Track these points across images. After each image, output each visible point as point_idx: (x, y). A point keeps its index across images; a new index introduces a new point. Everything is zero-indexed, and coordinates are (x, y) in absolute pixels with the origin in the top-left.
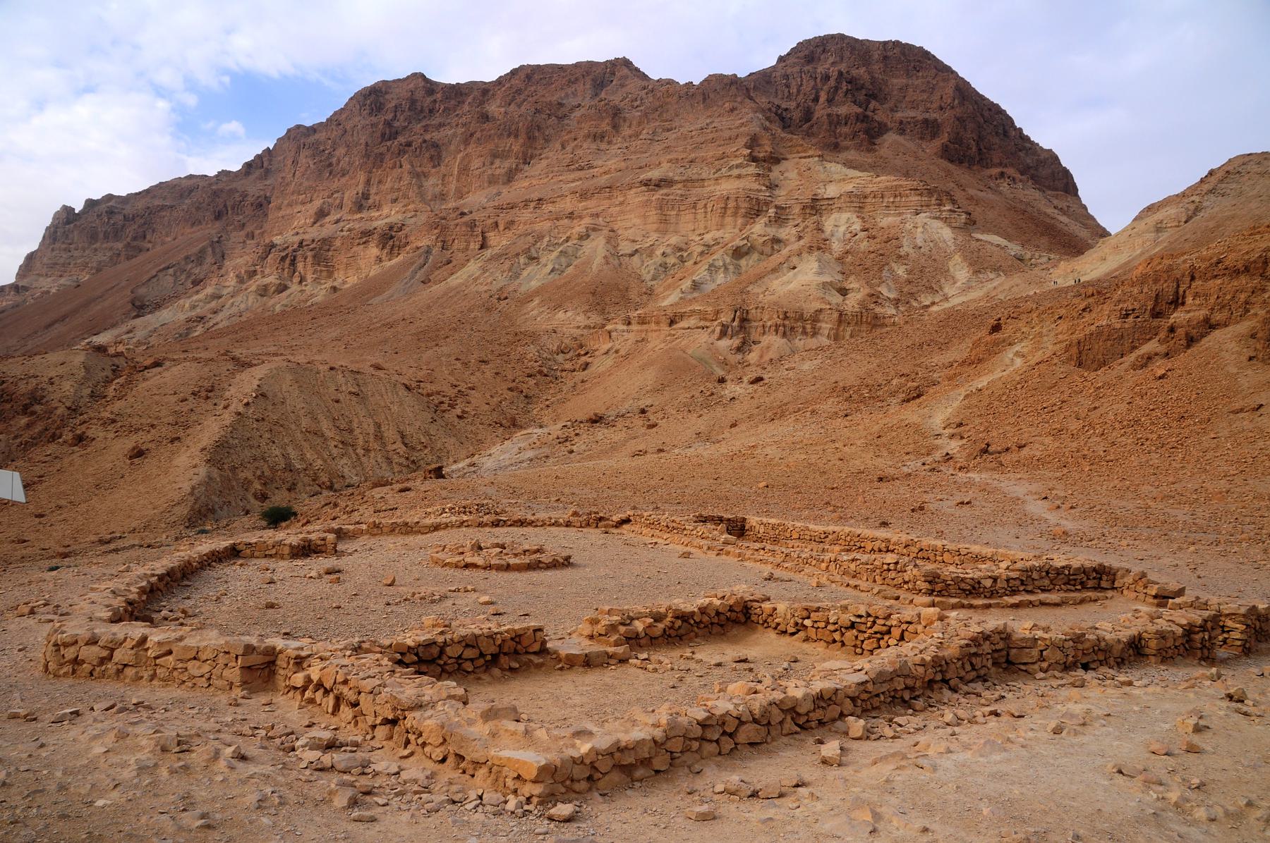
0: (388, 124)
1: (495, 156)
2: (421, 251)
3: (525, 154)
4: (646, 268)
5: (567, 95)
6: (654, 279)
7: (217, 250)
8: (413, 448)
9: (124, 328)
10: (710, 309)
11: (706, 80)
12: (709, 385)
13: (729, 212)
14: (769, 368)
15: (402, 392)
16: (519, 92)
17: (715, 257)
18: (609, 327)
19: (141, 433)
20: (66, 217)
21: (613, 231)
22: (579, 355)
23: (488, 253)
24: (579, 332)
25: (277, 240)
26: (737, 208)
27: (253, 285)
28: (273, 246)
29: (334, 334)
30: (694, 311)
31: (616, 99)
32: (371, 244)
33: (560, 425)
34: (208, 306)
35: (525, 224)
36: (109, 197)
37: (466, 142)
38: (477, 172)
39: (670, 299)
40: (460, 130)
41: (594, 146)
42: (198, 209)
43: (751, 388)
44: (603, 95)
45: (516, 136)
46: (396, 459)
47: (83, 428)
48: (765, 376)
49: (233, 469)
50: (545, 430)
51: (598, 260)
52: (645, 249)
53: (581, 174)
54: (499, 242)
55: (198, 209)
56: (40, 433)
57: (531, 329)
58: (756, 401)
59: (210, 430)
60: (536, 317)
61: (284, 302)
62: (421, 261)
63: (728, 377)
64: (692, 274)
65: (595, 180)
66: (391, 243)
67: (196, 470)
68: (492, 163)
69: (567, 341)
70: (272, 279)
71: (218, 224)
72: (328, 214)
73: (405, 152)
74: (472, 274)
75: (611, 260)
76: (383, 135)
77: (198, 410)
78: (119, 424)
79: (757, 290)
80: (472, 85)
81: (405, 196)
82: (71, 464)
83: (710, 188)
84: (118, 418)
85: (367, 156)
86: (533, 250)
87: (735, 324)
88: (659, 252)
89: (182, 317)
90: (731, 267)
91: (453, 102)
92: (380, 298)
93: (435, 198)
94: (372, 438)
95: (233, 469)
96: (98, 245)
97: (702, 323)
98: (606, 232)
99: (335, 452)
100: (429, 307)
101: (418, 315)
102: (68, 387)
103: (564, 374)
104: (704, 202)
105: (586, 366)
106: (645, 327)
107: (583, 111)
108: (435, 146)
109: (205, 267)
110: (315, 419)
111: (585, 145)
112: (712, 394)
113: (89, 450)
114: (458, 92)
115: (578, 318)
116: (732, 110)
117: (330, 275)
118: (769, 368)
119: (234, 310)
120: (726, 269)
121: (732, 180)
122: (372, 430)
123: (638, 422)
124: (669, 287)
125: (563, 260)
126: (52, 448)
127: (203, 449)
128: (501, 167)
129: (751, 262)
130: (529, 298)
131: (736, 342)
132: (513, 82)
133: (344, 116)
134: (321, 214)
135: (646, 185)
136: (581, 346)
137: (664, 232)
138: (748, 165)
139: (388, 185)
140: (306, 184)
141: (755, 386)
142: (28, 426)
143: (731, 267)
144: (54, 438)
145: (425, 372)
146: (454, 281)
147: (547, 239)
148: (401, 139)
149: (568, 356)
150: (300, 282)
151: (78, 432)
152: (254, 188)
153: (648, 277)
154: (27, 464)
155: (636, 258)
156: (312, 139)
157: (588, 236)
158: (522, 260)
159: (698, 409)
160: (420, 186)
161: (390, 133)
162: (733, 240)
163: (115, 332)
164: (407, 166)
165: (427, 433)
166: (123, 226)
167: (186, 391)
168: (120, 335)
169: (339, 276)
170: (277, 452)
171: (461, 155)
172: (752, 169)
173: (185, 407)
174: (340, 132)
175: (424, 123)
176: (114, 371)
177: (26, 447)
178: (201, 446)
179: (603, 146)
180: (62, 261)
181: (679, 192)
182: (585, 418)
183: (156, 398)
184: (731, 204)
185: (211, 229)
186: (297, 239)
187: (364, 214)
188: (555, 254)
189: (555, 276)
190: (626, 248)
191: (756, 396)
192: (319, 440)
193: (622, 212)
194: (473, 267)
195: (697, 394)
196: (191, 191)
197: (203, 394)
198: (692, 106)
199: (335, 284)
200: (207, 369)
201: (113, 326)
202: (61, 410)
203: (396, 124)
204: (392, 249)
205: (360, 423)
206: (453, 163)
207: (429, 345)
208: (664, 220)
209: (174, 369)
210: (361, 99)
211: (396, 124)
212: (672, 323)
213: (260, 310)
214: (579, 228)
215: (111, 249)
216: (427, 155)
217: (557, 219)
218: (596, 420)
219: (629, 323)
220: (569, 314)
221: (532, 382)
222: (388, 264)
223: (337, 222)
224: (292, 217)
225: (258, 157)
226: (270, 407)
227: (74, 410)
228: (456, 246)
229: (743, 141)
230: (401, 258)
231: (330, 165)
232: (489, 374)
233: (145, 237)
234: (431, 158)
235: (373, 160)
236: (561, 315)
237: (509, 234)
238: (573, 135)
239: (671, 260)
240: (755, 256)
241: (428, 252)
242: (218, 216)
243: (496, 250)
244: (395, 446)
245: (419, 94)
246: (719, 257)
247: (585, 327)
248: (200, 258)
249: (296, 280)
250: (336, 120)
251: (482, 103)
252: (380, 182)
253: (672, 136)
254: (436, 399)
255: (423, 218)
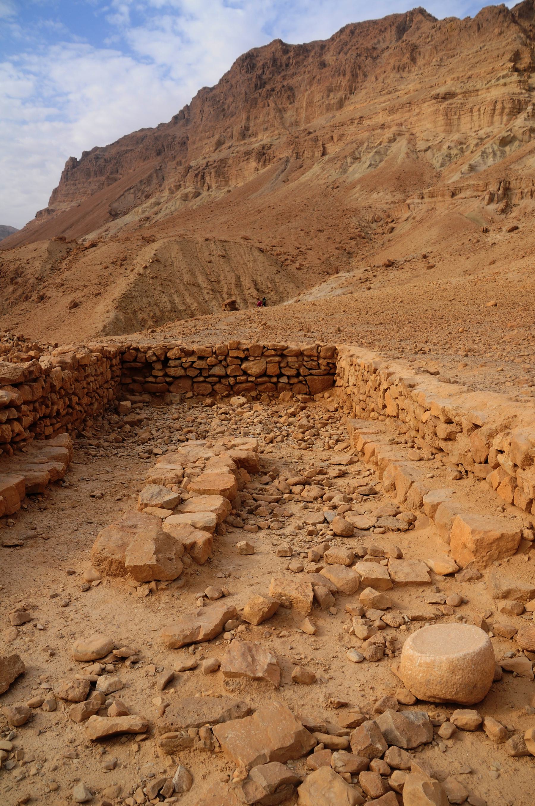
0: (259, 77)
1: (330, 90)
2: (282, 160)
3: (350, 87)
4: (435, 160)
5: (379, 42)
6: (442, 165)
7: (160, 175)
8: (263, 292)
9: (104, 228)
10: (481, 183)
11: (481, 13)
12: (476, 235)
13: (497, 112)
14: (523, 219)
15: (257, 253)
16: (346, 44)
17: (486, 146)
18: (408, 202)
19: (78, 291)
20: (73, 164)
21: (412, 134)
22: (387, 223)
23: (326, 158)
24: (388, 206)
25: (193, 163)
26: (503, 108)
27: (179, 194)
28: (190, 167)
29: (223, 220)
30: (469, 185)
31: (414, 39)
32: (252, 160)
33: (362, 270)
34: (153, 210)
35: (351, 135)
36: (96, 149)
37: (311, 83)
38: (319, 103)
39: (453, 178)
40: (307, 76)
41: (398, 76)
42: (147, 149)
43: (509, 235)
44: (404, 37)
45: (344, 75)
46: (250, 300)
47: (44, 291)
48: (519, 226)
49: (135, 312)
50: (351, 274)
51: (402, 155)
52: (436, 145)
53: (389, 96)
54: (333, 149)
55: (147, 149)
56: (20, 296)
57: (354, 207)
58: (512, 245)
59: (121, 286)
60: (358, 198)
61: (199, 204)
62: (283, 167)
63: (491, 228)
64: (470, 160)
65: (399, 99)
66: (264, 158)
67: (108, 315)
68: (328, 96)
69: (379, 213)
70: (190, 189)
71: (159, 158)
72: (224, 143)
73: (271, 95)
74: (316, 174)
75: (411, 155)
76: (256, 86)
77: (115, 274)
78: (66, 286)
79: (517, 167)
80: (314, 44)
81: (273, 126)
82: (35, 315)
83: (483, 94)
84: (65, 283)
85: (246, 101)
86: (356, 153)
87: (501, 192)
88: (445, 147)
89: (137, 218)
90: (498, 153)
91: (301, 57)
92: (255, 195)
93: (292, 125)
94: (233, 286)
95: (135, 312)
96: (91, 180)
97: (475, 194)
98: (407, 135)
99: (207, 297)
100: (286, 197)
101: (279, 203)
102: (37, 264)
103: (376, 236)
104: (478, 107)
105: (392, 229)
106: (434, 199)
107: (390, 51)
108: (291, 89)
109: (152, 186)
110: (193, 275)
111: (392, 75)
112: (478, 241)
113: (47, 304)
114: (303, 50)
115: (387, 197)
116: (500, 34)
117: (227, 183)
118: (523, 219)
119: (168, 211)
120: (495, 154)
121: (499, 88)
122: (233, 281)
123: (421, 264)
124: (452, 171)
125: (377, 158)
126: (26, 305)
127: (114, 300)
128: (334, 98)
129: (513, 148)
130: (353, 186)
131: (501, 205)
132: (341, 37)
133: (230, 76)
134: (219, 144)
135: (435, 98)
136: (389, 216)
137: (449, 132)
138: (511, 75)
139: (261, 119)
140: (210, 124)
141: (512, 234)
142: (14, 292)
143: (498, 153)
144: (27, 298)
145: (278, 240)
146: (304, 179)
147: (366, 144)
148: (268, 87)
149: (380, 224)
150: (208, 189)
151: (41, 294)
152: (179, 132)
153: (437, 165)
154: (10, 317)
155: (429, 152)
156: (211, 94)
157: (395, 140)
158: (349, 160)
159: (466, 253)
160: (282, 118)
161: (261, 84)
162: (500, 132)
163: (98, 231)
164: (272, 105)
165: (273, 281)
166: (105, 166)
167: (108, 262)
168: (101, 233)
169: (232, 183)
170: (166, 299)
171: (308, 92)
172: (515, 77)
173: (106, 272)
174: (229, 87)
175: (282, 74)
176: (68, 252)
177: (12, 305)
178: (113, 298)
179: (405, 75)
180: (71, 192)
181: (460, 101)
182: (381, 263)
183: (89, 267)
184: (499, 106)
185: (155, 162)
186: (205, 161)
187: (247, 141)
188: (372, 154)
189: (371, 169)
190: (421, 145)
191: (512, 241)
192: (196, 290)
193: (419, 120)
194: (316, 168)
195: (466, 242)
196: (143, 139)
197: (119, 263)
198: (469, 35)
199: (230, 189)
200: (123, 246)
201: (98, 228)
202: (32, 280)
203: (264, 77)
204: (265, 162)
205: (226, 276)
206: (302, 99)
207: (284, 222)
208: (449, 124)
209: (103, 248)
210: (241, 62)
211: (264, 77)
212: (453, 195)
213: (184, 210)
214: (388, 134)
215: (99, 181)
216: (286, 96)
217: (373, 130)
218: (390, 265)
219: (423, 198)
220: (380, 194)
221: (353, 243)
222: (262, 171)
223: (230, 147)
224: (202, 147)
225: (182, 112)
226: (162, 269)
227: (40, 279)
228: (305, 155)
229: (508, 57)
230: (269, 167)
231: (224, 110)
232: (323, 239)
233: (118, 172)
234: (289, 97)
235: (251, 103)
236: (375, 196)
237: (341, 144)
238: (383, 69)
239: (454, 152)
240: (517, 143)
241: (287, 161)
242: (159, 153)
243: (332, 156)
244: (249, 291)
245: (279, 55)
246: (490, 145)
247: (392, 203)
248: (149, 181)
249: (206, 188)
250: (225, 80)
251: (321, 55)
252: (256, 118)
253: (455, 60)
254: (283, 258)
255: (284, 139)
